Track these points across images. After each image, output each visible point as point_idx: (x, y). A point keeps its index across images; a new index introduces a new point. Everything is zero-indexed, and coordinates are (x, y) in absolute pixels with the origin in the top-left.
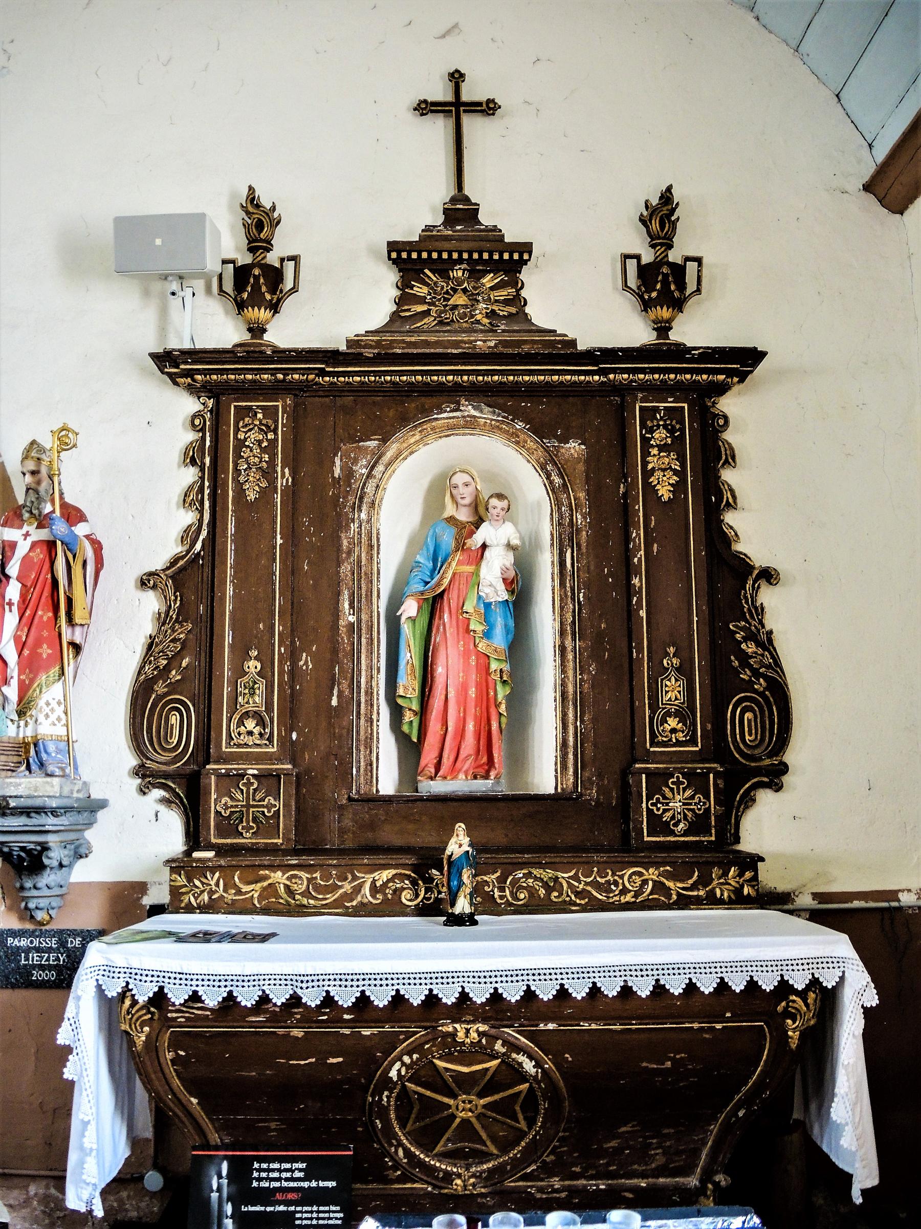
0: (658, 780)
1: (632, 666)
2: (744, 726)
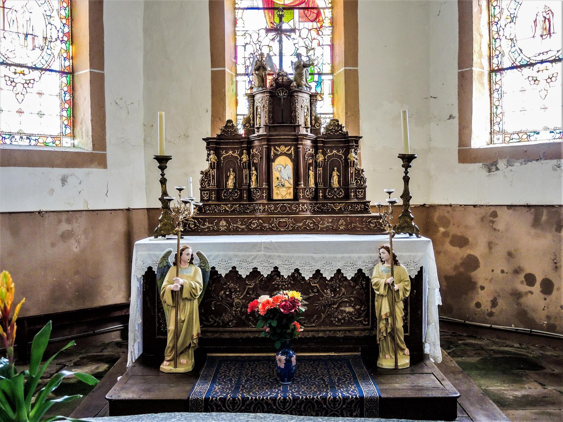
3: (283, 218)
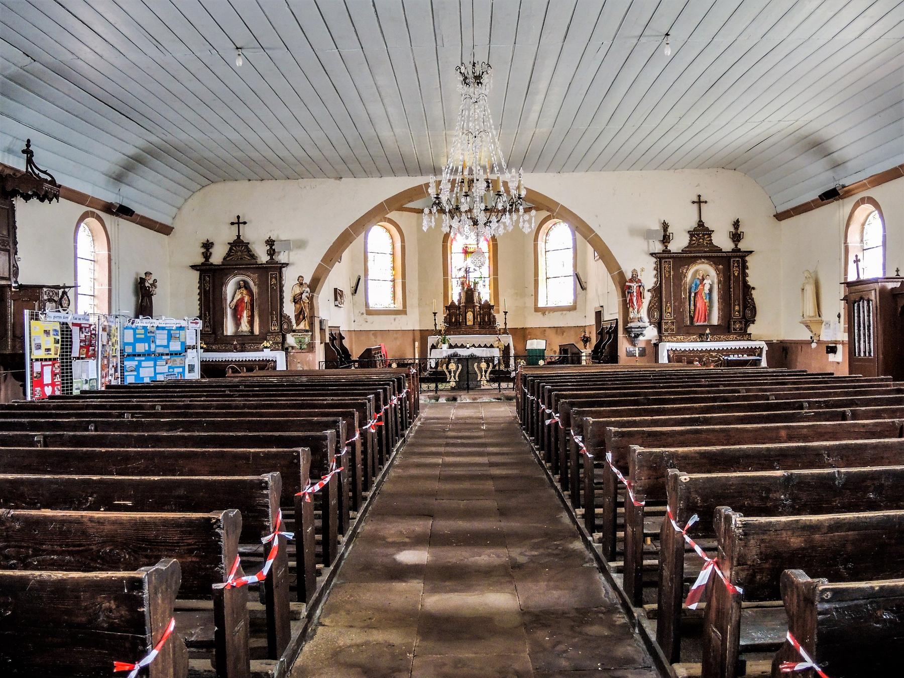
0: (735, 322)
1: (730, 304)
2: (748, 312)
3: (469, 331)
